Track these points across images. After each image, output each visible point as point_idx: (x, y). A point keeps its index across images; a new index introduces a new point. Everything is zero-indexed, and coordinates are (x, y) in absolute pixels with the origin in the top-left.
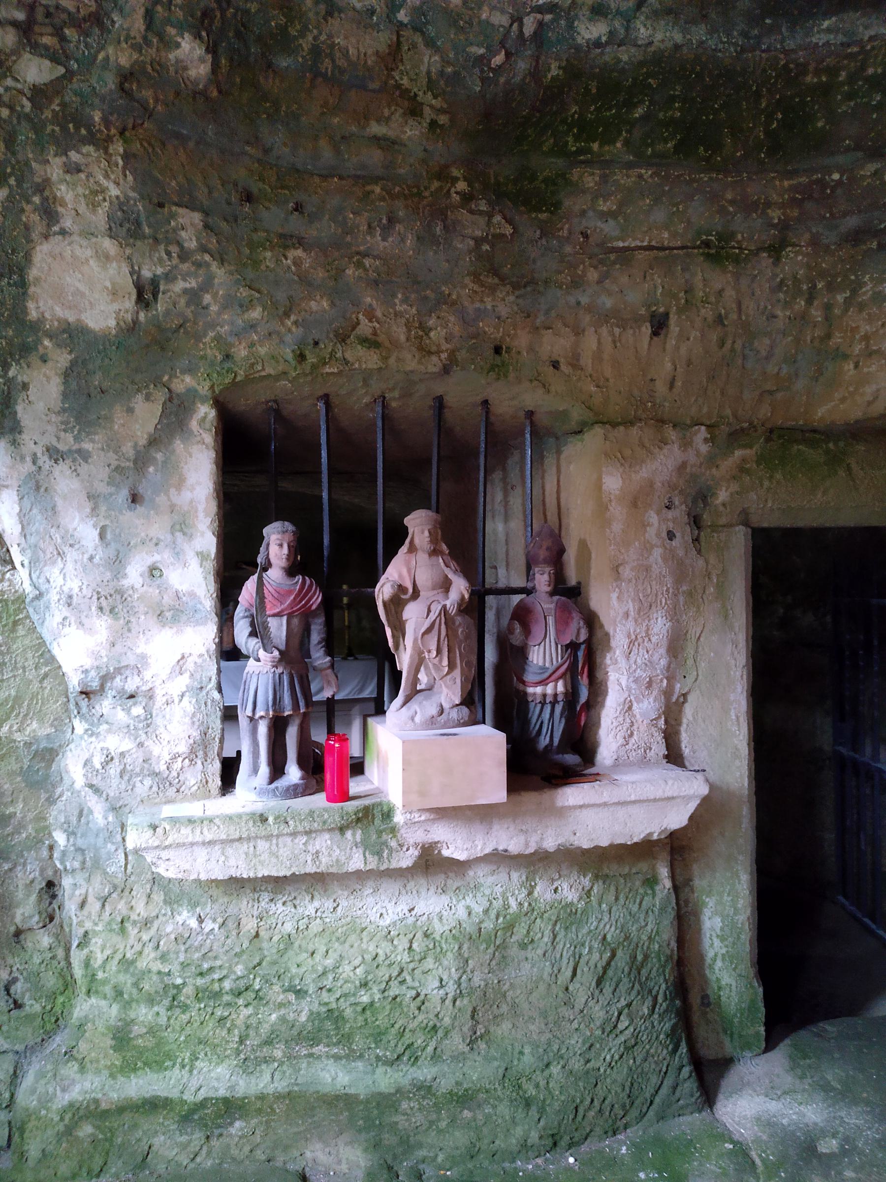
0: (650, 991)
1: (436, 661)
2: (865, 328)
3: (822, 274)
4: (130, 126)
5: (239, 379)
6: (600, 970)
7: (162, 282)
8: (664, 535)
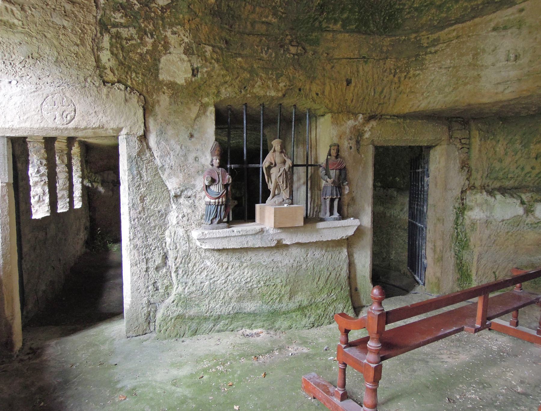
0: (341, 284)
1: (282, 185)
2: (410, 85)
3: (398, 67)
4: (191, 19)
5: (222, 99)
6: (327, 278)
7: (200, 69)
8: (349, 148)
